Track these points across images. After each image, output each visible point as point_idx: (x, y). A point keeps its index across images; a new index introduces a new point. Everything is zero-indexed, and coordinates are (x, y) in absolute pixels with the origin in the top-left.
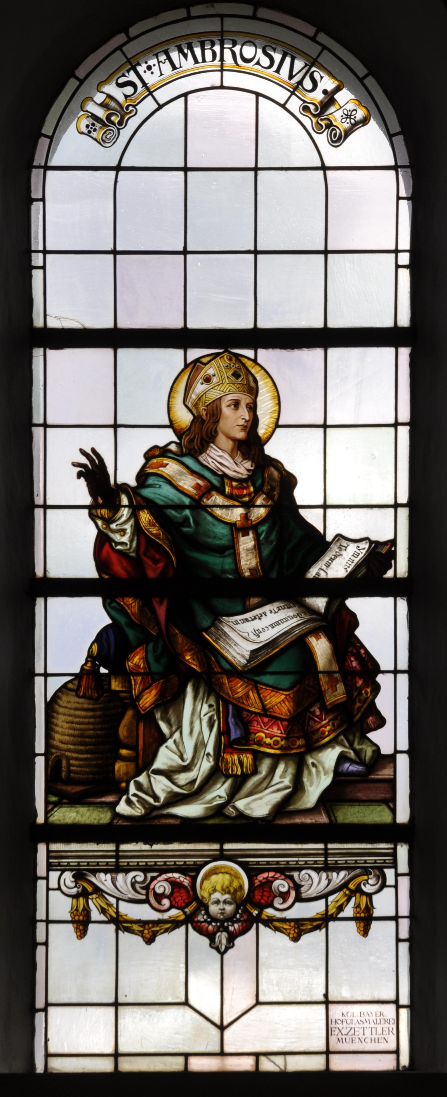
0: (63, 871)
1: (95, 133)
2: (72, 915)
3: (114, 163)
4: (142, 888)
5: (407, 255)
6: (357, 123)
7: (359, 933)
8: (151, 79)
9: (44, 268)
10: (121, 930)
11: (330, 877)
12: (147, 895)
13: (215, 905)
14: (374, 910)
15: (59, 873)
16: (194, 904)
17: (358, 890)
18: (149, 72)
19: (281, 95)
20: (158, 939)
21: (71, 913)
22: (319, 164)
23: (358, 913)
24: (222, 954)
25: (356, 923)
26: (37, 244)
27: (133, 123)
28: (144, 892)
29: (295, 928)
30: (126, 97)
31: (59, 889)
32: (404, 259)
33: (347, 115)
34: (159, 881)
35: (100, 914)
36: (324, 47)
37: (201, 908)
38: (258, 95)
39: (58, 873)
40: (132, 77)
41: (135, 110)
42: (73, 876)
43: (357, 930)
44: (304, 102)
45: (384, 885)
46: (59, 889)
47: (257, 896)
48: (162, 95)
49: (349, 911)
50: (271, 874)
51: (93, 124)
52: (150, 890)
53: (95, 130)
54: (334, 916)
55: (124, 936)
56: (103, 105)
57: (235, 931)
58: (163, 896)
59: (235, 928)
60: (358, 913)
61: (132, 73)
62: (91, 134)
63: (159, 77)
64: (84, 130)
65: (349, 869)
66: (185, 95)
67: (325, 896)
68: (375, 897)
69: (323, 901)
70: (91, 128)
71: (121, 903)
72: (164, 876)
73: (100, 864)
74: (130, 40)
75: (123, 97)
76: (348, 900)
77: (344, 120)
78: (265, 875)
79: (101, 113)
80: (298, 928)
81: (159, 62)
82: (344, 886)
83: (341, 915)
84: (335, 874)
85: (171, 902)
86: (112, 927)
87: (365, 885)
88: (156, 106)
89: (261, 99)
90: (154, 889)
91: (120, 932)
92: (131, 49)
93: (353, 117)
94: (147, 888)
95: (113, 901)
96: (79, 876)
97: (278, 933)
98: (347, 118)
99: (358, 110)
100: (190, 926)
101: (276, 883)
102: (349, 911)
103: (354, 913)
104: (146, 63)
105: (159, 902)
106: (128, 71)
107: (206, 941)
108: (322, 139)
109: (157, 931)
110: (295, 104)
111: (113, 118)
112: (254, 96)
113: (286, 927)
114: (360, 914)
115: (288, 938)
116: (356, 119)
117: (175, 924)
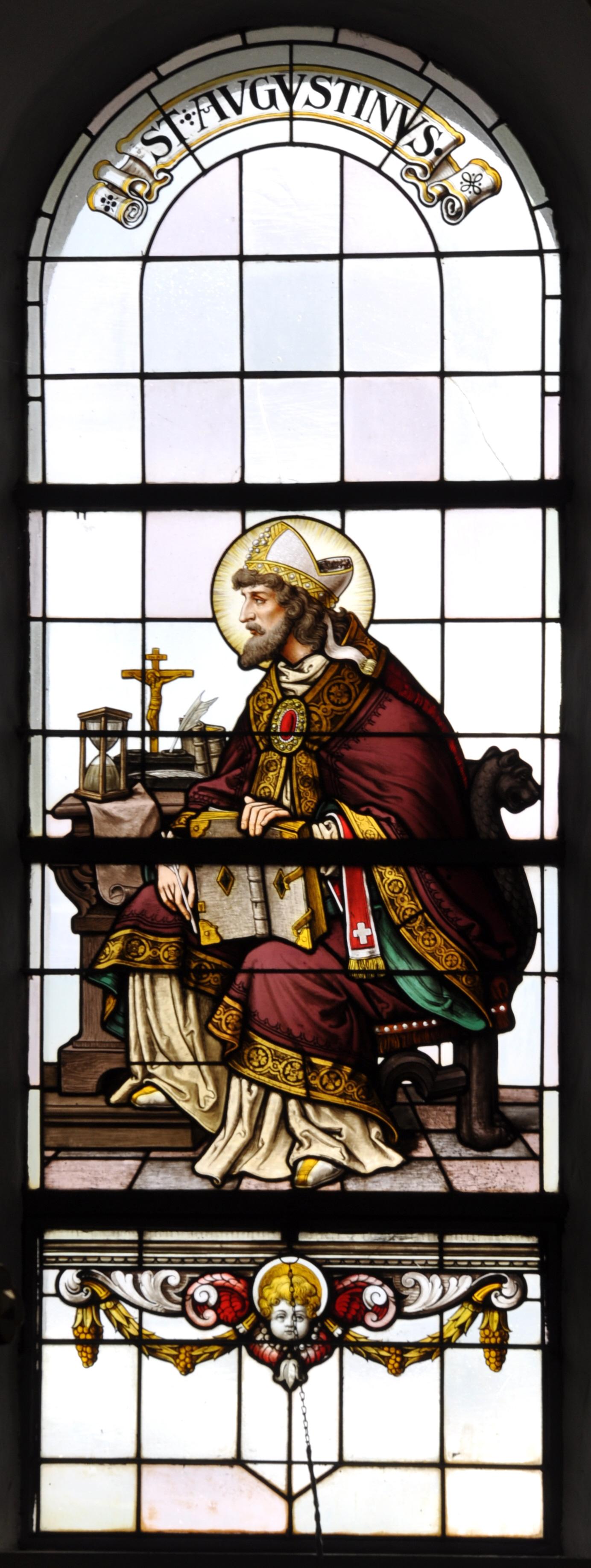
0: (62, 1270)
1: (115, 209)
2: (76, 1332)
3: (140, 251)
4: (177, 1294)
5: (556, 379)
6: (480, 193)
7: (489, 1366)
8: (190, 131)
9: (42, 399)
10: (145, 1354)
11: (446, 1285)
12: (183, 1304)
13: (280, 1320)
14: (510, 1334)
15: (57, 1272)
16: (251, 1319)
17: (486, 1306)
18: (187, 122)
19: (376, 154)
20: (198, 1368)
21: (75, 1329)
22: (431, 249)
23: (487, 1337)
24: (289, 1391)
25: (485, 1352)
26: (33, 368)
27: (167, 195)
28: (179, 1299)
29: (397, 1355)
30: (157, 158)
31: (58, 1294)
32: (553, 384)
33: (470, 182)
34: (202, 1285)
35: (116, 1331)
36: (436, 86)
37: (261, 1324)
38: (343, 154)
39: (56, 1272)
40: (165, 130)
41: (169, 177)
42: (79, 1276)
43: (486, 1363)
44: (407, 163)
45: (523, 1298)
46: (58, 1294)
47: (340, 1308)
48: (207, 156)
49: (474, 1335)
50: (363, 1277)
51: (111, 197)
52: (188, 1297)
53: (114, 204)
54: (453, 1340)
55: (150, 1363)
56: (125, 171)
57: (308, 1360)
58: (205, 1306)
59: (308, 1355)
60: (487, 1337)
61: (342, 86)
62: (110, 212)
63: (199, 132)
64: (99, 205)
65: (472, 1273)
66: (239, 155)
67: (439, 1311)
68: (510, 1314)
69: (436, 1319)
70: (108, 203)
71: (146, 1315)
72: (208, 1278)
73: (116, 1260)
74: (161, 79)
75: (153, 159)
76: (473, 1317)
77: (465, 188)
78: (354, 1278)
79: (119, 180)
80: (401, 1356)
81: (199, 111)
82: (466, 1298)
83: (463, 1339)
84: (453, 1280)
85: (218, 1315)
86: (131, 1351)
87: (496, 1296)
88: (199, 171)
89: (346, 159)
90: (192, 1296)
91: (144, 1357)
92: (162, 93)
93: (476, 184)
94: (183, 1294)
95: (134, 1313)
96: (86, 1276)
97: (370, 1362)
98: (470, 186)
99: (484, 173)
100: (244, 1350)
101: (369, 1291)
102: (474, 1335)
103: (482, 1337)
104: (184, 111)
105: (199, 1314)
106: (159, 123)
107: (267, 1372)
108: (434, 214)
109: (198, 1356)
110: (394, 167)
111: (139, 188)
112: (337, 156)
113: (383, 1353)
114: (490, 1338)
115: (385, 1369)
116: (481, 187)
117: (224, 1345)
